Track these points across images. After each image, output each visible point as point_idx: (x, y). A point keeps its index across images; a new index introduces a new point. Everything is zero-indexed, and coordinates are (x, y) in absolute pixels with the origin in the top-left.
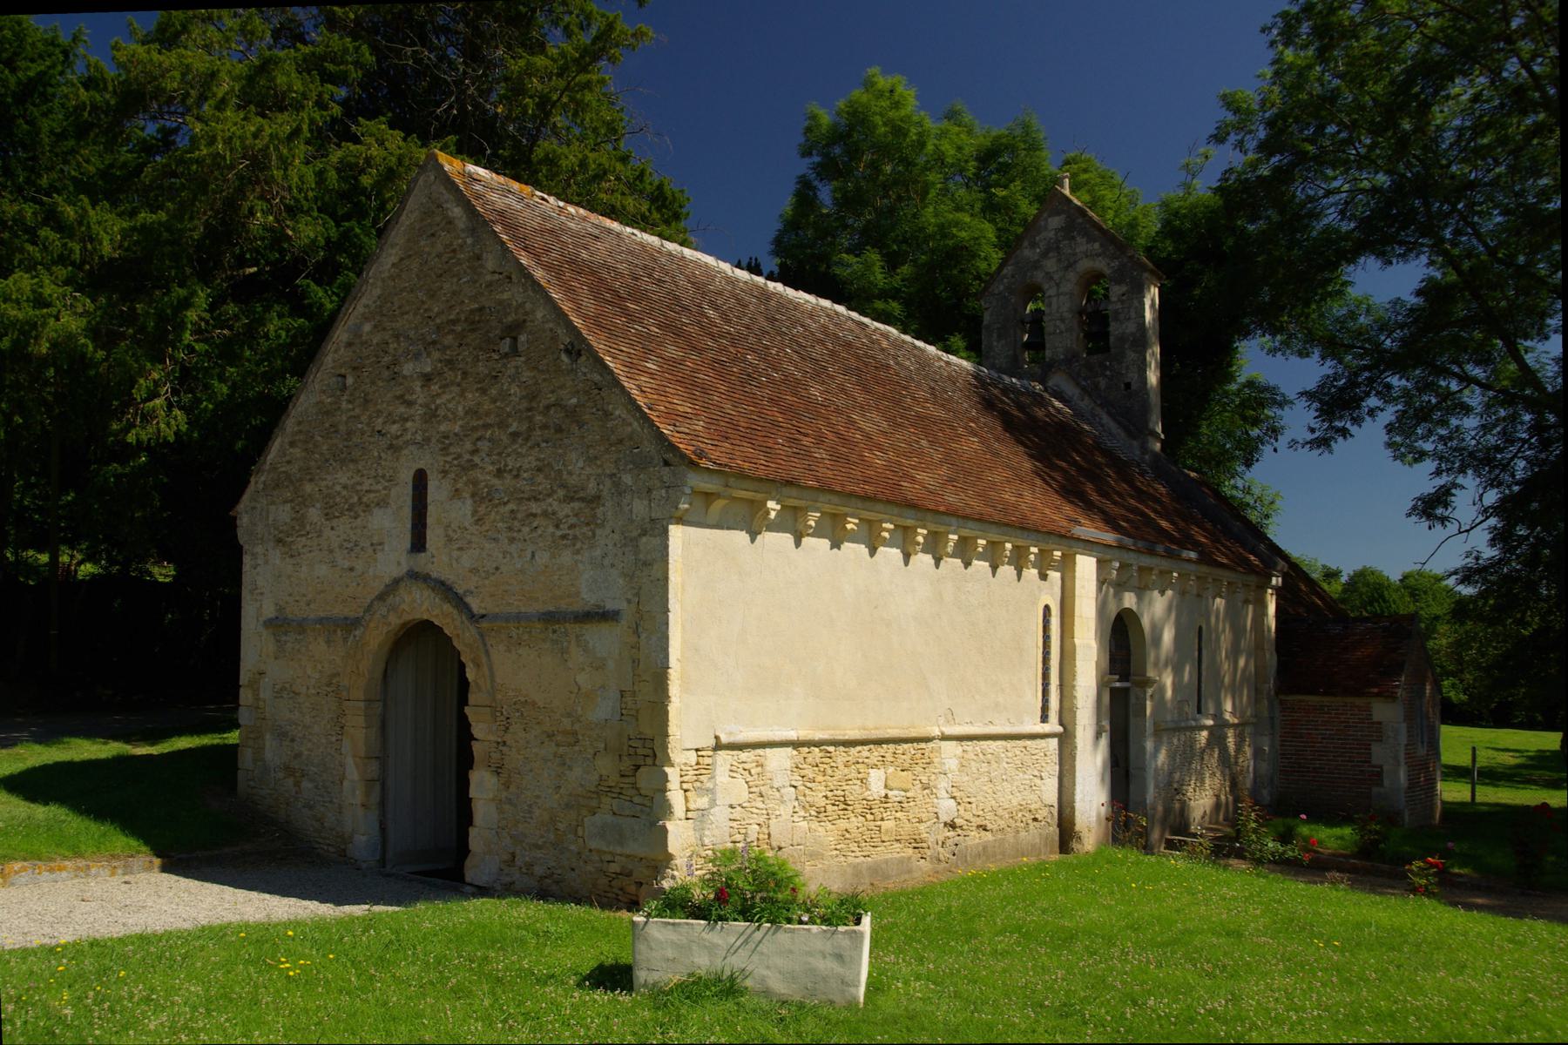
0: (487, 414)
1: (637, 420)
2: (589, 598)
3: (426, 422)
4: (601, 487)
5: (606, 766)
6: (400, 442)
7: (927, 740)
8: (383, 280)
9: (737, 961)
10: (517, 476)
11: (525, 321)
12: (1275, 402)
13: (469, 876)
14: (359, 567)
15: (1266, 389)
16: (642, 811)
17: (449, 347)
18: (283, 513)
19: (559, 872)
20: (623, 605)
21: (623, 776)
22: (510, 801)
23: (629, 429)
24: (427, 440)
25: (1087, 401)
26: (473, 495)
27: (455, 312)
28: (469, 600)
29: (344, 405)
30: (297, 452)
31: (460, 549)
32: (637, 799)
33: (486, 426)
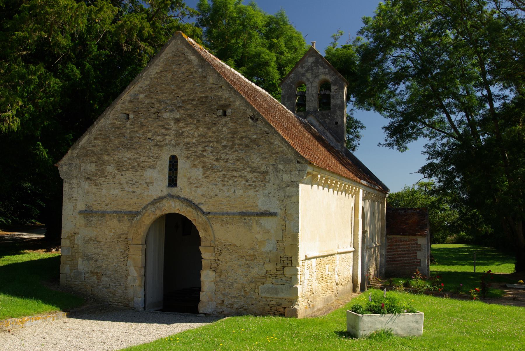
0: (210, 137)
1: (286, 146)
2: (262, 207)
3: (177, 137)
4: (268, 168)
5: (270, 267)
6: (162, 143)
7: (334, 254)
8: (151, 78)
9: (389, 326)
10: (227, 162)
11: (230, 105)
12: (359, 127)
13: (201, 310)
14: (138, 191)
15: (356, 122)
16: (286, 282)
17: (189, 109)
18: (91, 168)
19: (247, 306)
20: (279, 211)
21: (277, 270)
22: (222, 281)
23: (282, 149)
24: (179, 144)
25: (321, 127)
26: (203, 167)
27: (192, 97)
28: (201, 206)
29: (128, 126)
30: (99, 142)
31: (197, 187)
32: (284, 278)
33: (210, 142)
